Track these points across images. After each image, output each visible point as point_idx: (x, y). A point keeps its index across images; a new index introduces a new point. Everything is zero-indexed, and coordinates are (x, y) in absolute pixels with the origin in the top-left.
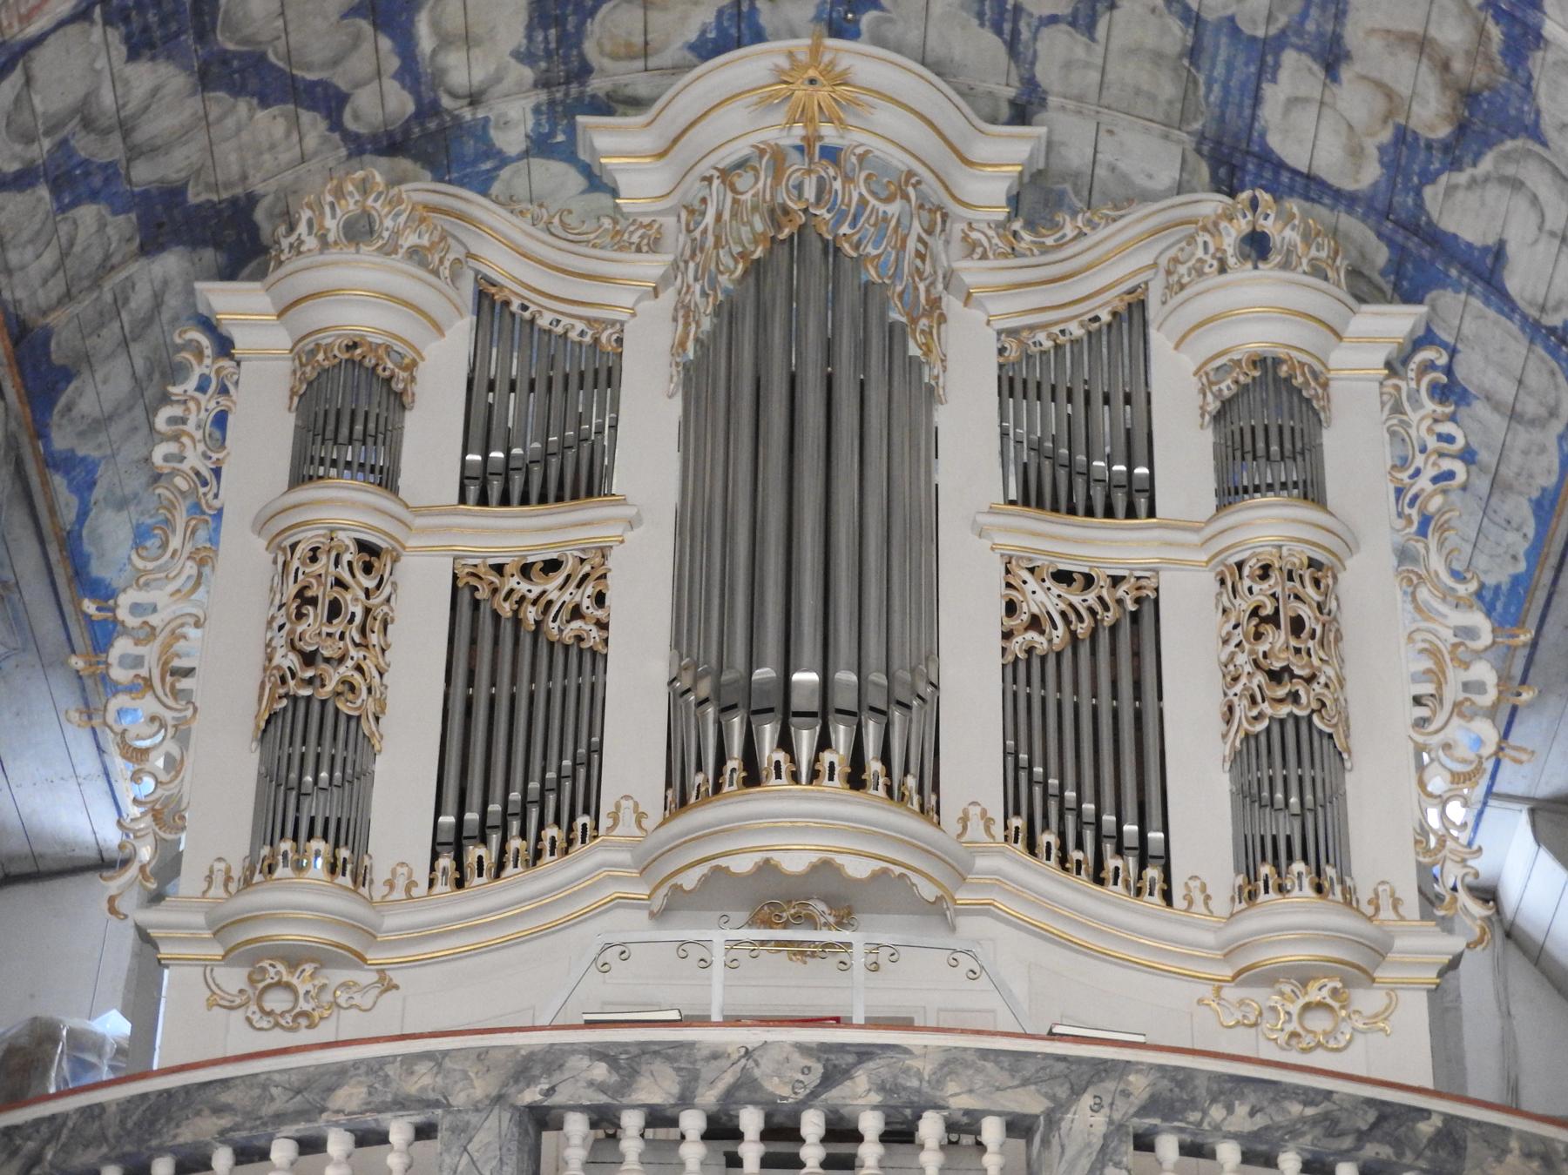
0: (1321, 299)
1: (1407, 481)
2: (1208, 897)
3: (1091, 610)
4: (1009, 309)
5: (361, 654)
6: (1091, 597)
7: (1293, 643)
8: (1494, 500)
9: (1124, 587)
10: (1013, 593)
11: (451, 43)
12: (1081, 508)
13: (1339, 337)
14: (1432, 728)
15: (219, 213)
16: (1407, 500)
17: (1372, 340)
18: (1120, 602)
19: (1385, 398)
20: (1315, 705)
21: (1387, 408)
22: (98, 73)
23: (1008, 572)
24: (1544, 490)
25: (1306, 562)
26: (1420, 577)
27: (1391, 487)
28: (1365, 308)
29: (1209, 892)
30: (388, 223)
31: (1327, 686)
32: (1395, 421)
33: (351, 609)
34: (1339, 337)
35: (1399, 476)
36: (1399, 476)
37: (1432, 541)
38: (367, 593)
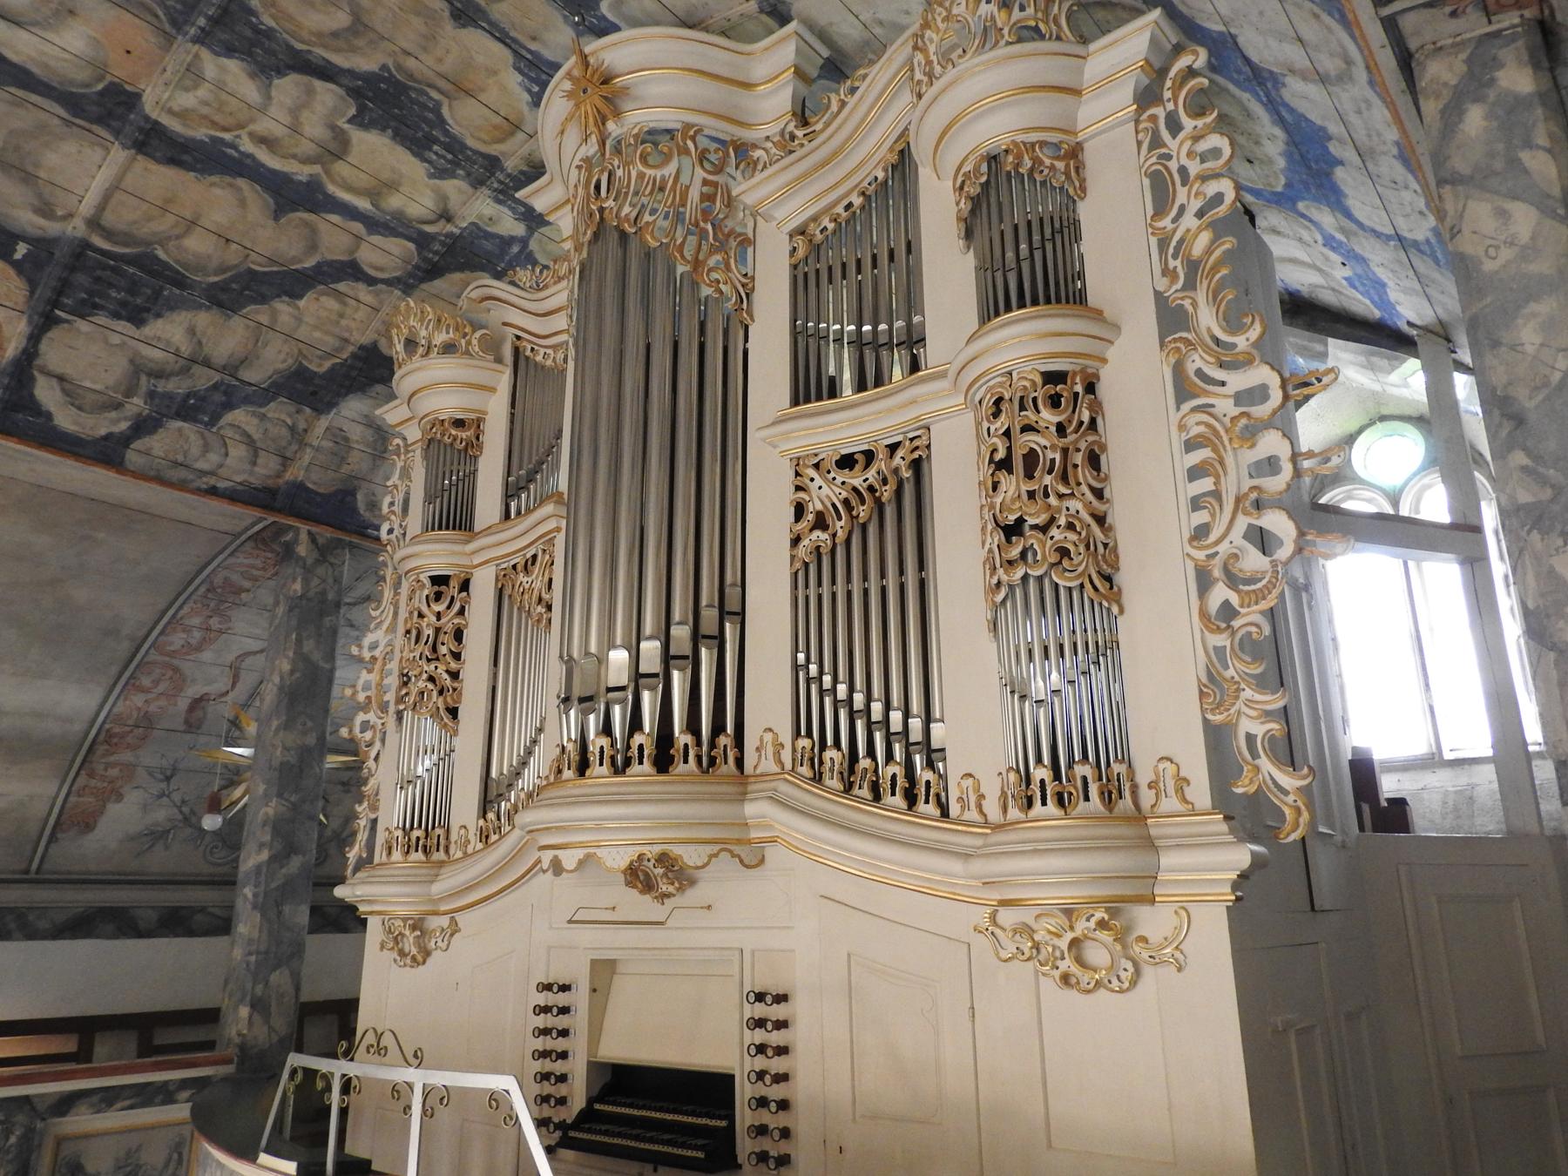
0: (1036, 64)
1: (1171, 227)
2: (982, 796)
3: (871, 489)
4: (795, 210)
5: (432, 667)
6: (871, 474)
7: (1025, 487)
8: (1370, 166)
9: (900, 453)
10: (801, 495)
11: (379, 194)
12: (1041, 298)
13: (1077, 92)
14: (1212, 538)
15: (351, 367)
16: (1171, 250)
17: (1109, 80)
18: (896, 471)
19: (1141, 136)
20: (1054, 558)
21: (1145, 146)
22: (122, 345)
23: (797, 474)
24: (1397, 143)
25: (1039, 380)
26: (1187, 342)
27: (1154, 241)
28: (1093, 47)
29: (982, 790)
30: (423, 333)
31: (1071, 526)
32: (1154, 160)
33: (1178, 263)
34: (1077, 92)
35: (1160, 224)
36: (1160, 224)
37: (1201, 296)
38: (439, 616)
